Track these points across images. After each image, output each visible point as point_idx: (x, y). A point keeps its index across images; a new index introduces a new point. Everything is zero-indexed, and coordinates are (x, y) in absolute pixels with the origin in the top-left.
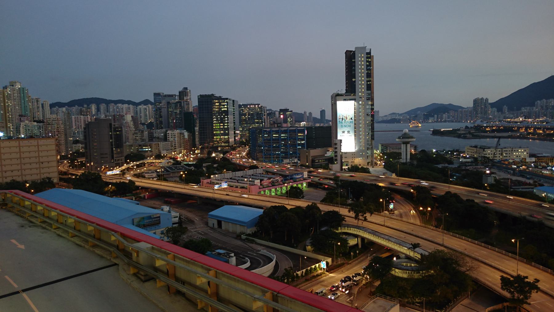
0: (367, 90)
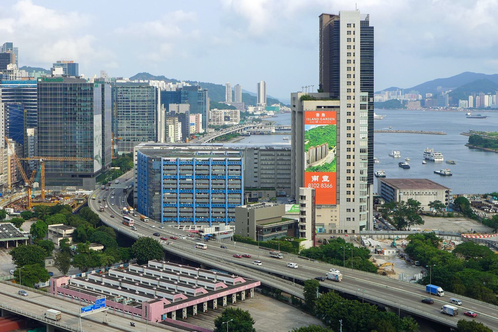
0: (362, 90)
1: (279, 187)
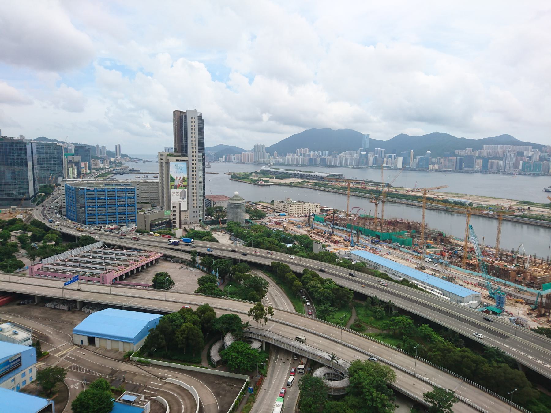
0: (199, 152)
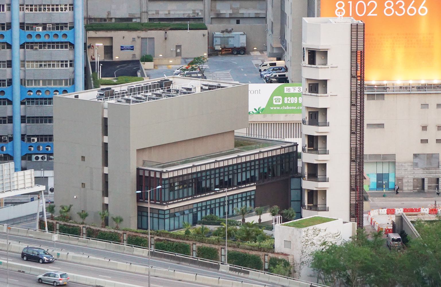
1: (219, 17)
